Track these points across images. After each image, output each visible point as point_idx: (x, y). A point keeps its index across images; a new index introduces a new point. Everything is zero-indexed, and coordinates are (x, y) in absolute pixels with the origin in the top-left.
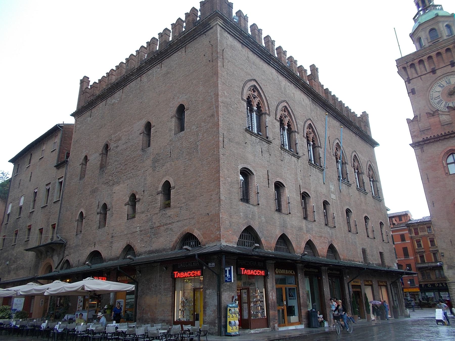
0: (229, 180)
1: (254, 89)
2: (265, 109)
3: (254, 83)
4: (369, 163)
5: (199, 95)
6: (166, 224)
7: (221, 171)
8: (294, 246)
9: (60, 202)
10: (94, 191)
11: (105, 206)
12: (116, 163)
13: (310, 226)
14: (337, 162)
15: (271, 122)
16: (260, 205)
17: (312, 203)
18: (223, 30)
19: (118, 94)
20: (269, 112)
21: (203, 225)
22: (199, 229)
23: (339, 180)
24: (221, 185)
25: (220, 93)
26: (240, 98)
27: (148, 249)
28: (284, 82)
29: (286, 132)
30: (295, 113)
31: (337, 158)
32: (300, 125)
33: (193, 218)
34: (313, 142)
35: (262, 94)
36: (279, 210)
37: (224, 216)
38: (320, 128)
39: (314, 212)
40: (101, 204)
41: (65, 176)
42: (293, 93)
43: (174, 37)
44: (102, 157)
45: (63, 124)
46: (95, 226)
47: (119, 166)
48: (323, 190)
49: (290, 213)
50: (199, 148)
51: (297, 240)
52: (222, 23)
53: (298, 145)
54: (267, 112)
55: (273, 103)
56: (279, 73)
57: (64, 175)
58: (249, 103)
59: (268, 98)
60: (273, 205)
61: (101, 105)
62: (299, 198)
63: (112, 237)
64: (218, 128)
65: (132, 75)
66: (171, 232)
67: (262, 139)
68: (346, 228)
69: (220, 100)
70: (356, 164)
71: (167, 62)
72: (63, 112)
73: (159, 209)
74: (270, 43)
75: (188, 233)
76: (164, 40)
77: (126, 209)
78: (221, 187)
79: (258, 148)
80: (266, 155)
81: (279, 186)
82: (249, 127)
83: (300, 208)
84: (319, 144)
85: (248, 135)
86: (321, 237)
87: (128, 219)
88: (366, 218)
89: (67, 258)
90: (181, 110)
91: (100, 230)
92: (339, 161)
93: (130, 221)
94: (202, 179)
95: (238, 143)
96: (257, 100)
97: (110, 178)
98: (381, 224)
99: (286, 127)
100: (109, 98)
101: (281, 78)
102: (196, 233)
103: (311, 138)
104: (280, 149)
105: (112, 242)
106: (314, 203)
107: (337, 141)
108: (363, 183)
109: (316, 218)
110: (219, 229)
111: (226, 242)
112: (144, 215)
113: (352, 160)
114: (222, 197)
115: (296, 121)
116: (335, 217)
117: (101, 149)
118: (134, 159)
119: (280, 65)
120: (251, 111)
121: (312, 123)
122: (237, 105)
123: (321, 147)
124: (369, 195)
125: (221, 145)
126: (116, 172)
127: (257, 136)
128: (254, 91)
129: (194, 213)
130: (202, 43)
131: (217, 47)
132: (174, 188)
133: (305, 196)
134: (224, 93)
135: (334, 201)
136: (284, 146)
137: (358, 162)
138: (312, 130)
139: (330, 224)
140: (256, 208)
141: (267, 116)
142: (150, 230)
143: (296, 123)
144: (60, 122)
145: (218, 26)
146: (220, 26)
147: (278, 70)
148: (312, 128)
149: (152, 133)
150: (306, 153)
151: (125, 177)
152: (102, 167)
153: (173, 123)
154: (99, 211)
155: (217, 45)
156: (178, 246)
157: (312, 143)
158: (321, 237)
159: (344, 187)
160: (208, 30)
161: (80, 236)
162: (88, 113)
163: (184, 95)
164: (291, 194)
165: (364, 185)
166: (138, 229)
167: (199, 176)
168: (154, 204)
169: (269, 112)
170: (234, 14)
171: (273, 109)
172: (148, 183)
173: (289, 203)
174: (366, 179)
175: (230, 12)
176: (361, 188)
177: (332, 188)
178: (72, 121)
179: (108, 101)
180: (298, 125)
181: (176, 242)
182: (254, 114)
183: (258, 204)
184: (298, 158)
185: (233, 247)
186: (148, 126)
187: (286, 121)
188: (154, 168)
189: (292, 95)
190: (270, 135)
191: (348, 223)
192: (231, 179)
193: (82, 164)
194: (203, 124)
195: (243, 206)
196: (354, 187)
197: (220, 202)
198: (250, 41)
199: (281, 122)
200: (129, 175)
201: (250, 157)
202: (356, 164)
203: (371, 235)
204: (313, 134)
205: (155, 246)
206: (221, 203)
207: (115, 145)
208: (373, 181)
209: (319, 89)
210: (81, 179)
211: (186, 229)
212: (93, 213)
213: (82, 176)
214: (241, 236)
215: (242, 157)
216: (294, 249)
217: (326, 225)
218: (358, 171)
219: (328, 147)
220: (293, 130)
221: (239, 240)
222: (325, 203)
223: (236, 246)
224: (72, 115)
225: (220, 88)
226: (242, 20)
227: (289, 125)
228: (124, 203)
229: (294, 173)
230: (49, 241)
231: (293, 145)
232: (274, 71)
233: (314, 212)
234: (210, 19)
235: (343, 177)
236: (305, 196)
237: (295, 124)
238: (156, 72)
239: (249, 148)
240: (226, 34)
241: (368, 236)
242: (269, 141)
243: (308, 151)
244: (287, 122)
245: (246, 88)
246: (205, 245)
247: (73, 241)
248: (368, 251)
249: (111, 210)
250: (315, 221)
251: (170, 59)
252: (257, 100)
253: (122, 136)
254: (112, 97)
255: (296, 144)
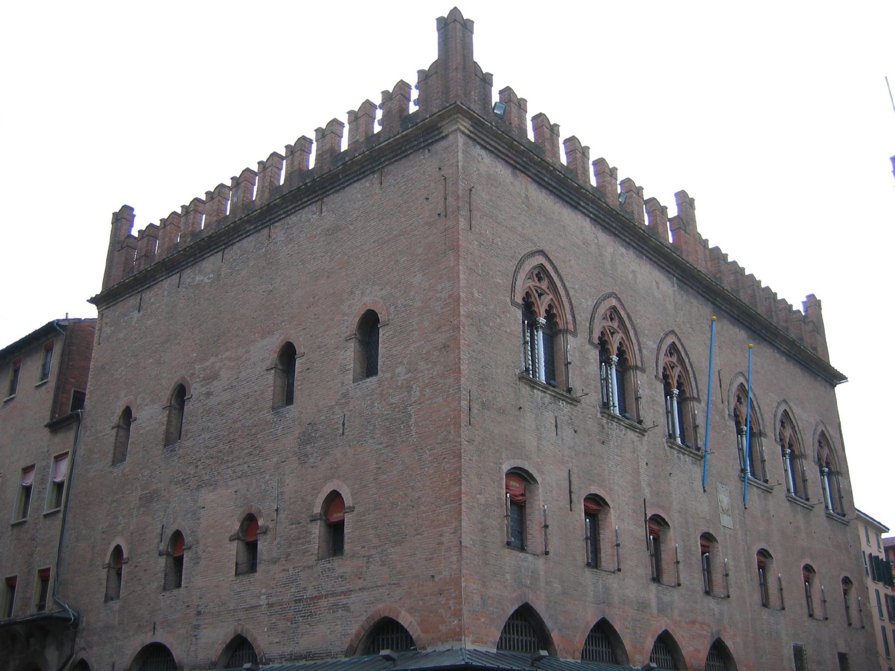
0: (482, 500)
1: (541, 273)
2: (565, 319)
3: (541, 260)
4: (821, 428)
5: (412, 293)
6: (334, 594)
7: (463, 480)
8: (628, 648)
9: (61, 515)
10: (148, 500)
11: (178, 537)
12: (206, 436)
13: (666, 599)
14: (740, 432)
15: (579, 350)
16: (551, 555)
17: (673, 541)
18: (471, 142)
19: (211, 263)
20: (575, 327)
21: (421, 603)
22: (412, 611)
23: (743, 479)
24: (463, 513)
25: (462, 295)
26: (508, 300)
27: (288, 650)
28: (611, 248)
29: (614, 370)
30: (638, 321)
31: (738, 424)
32: (648, 351)
33: (398, 585)
34: (678, 386)
35: (559, 285)
36: (594, 562)
37: (470, 585)
38: (696, 351)
39: (678, 562)
40: (169, 532)
41: (74, 452)
42: (634, 272)
43: (353, 144)
44: (169, 416)
45: (67, 319)
46: (155, 585)
47: (213, 442)
48: (703, 507)
49: (619, 570)
50: (413, 420)
51: (635, 633)
52: (468, 126)
53: (643, 403)
54: (571, 327)
55: (584, 304)
56: (598, 227)
57: (70, 450)
58: (528, 308)
59: (571, 293)
60: (581, 554)
61: (168, 284)
62: (641, 532)
63: (199, 613)
64: (458, 380)
65: (248, 221)
66: (345, 613)
67: (557, 397)
68: (757, 597)
69: (462, 312)
70: (788, 433)
71: (335, 201)
72: (71, 290)
73: (315, 558)
74: (579, 155)
75: (386, 618)
76: (327, 147)
77: (233, 550)
78: (464, 517)
79: (549, 416)
80: (567, 432)
81: (596, 507)
82: (527, 370)
83: (644, 556)
84: (695, 391)
85: (525, 389)
86: (693, 622)
87: (237, 574)
88: (808, 569)
89: (82, 655)
90: (370, 324)
91: (167, 594)
92: (745, 428)
93: (245, 579)
94: (417, 495)
95: (502, 411)
96: (546, 300)
97: (191, 470)
98: (846, 581)
99: (615, 358)
100: (188, 271)
101: (603, 238)
102: (406, 619)
103: (676, 379)
104: (599, 415)
105: (197, 627)
106: (680, 542)
107: (741, 380)
108: (805, 481)
109: (682, 576)
110: (458, 614)
111: (473, 642)
112: (275, 568)
113: (778, 425)
114: (466, 541)
115: (638, 340)
116: (731, 573)
117: (166, 394)
118: (253, 431)
119: (600, 207)
120: (531, 324)
121: (677, 343)
122: (500, 318)
123: (698, 400)
124: (819, 510)
125: (464, 417)
126: (207, 458)
127: (546, 388)
128: (540, 279)
129: (399, 573)
130: (420, 169)
131: (456, 183)
132: (352, 509)
133: (657, 525)
134: (472, 294)
135: (728, 531)
136: (608, 408)
137: (793, 428)
138: (678, 357)
139: (718, 590)
140: (540, 564)
141: (569, 337)
142: (293, 604)
143: (639, 345)
144: (57, 314)
145: (459, 135)
146: (463, 133)
147: (596, 220)
148: (678, 352)
149: (297, 370)
150: (662, 420)
151: (230, 471)
152: (173, 437)
153: (350, 354)
154: (162, 547)
155: (457, 180)
156: (361, 647)
157: (676, 391)
158: (693, 622)
159: (754, 494)
160: (437, 141)
161: (115, 605)
162: (133, 301)
163: (377, 288)
164: (623, 525)
165: (805, 487)
166: (263, 600)
167: (413, 488)
168: (302, 544)
169: (575, 327)
170: (495, 98)
171: (583, 317)
172: (290, 492)
173: (618, 545)
174: (810, 469)
175: (487, 96)
176: (799, 495)
177: (724, 499)
178: (91, 312)
179: (184, 276)
180: (644, 351)
181: (357, 635)
182: (540, 336)
183: (547, 553)
184: (643, 432)
185: (487, 654)
186: (288, 354)
187: (614, 343)
188: (303, 458)
189: (631, 276)
190: (575, 382)
191: (764, 585)
192: (486, 495)
193: (118, 426)
194: (422, 365)
195: (512, 558)
196: (780, 493)
197: (460, 550)
198: (531, 160)
199: (603, 346)
200: (240, 468)
201: (530, 441)
202: (788, 433)
203: (818, 612)
204: (679, 368)
205: (304, 644)
206: (465, 553)
207: (204, 390)
208: (830, 474)
209: (696, 251)
210: (114, 463)
211: (382, 608)
212: (147, 552)
213: (119, 456)
214: (508, 628)
215: (511, 443)
216: (626, 654)
217: (708, 593)
218: (793, 451)
219: (716, 397)
220: (632, 362)
221: (501, 638)
222: (708, 539)
223: (494, 651)
224: (92, 301)
225: (463, 283)
226: (514, 110)
227: (621, 353)
228: (228, 535)
229: (632, 471)
230: (32, 610)
231: (630, 400)
232: (586, 224)
233: (678, 562)
234: (441, 118)
235: (752, 467)
236: (657, 525)
237: (636, 348)
238: (310, 220)
239: (529, 420)
240: (478, 151)
241: (811, 615)
242: (573, 400)
243: (667, 412)
244: (616, 345)
245: (522, 275)
246: (424, 648)
247: (98, 616)
248: (809, 652)
249: (194, 548)
250: (679, 585)
251: (342, 194)
252: (546, 300)
253: (220, 368)
254: (197, 267)
255: (637, 399)
